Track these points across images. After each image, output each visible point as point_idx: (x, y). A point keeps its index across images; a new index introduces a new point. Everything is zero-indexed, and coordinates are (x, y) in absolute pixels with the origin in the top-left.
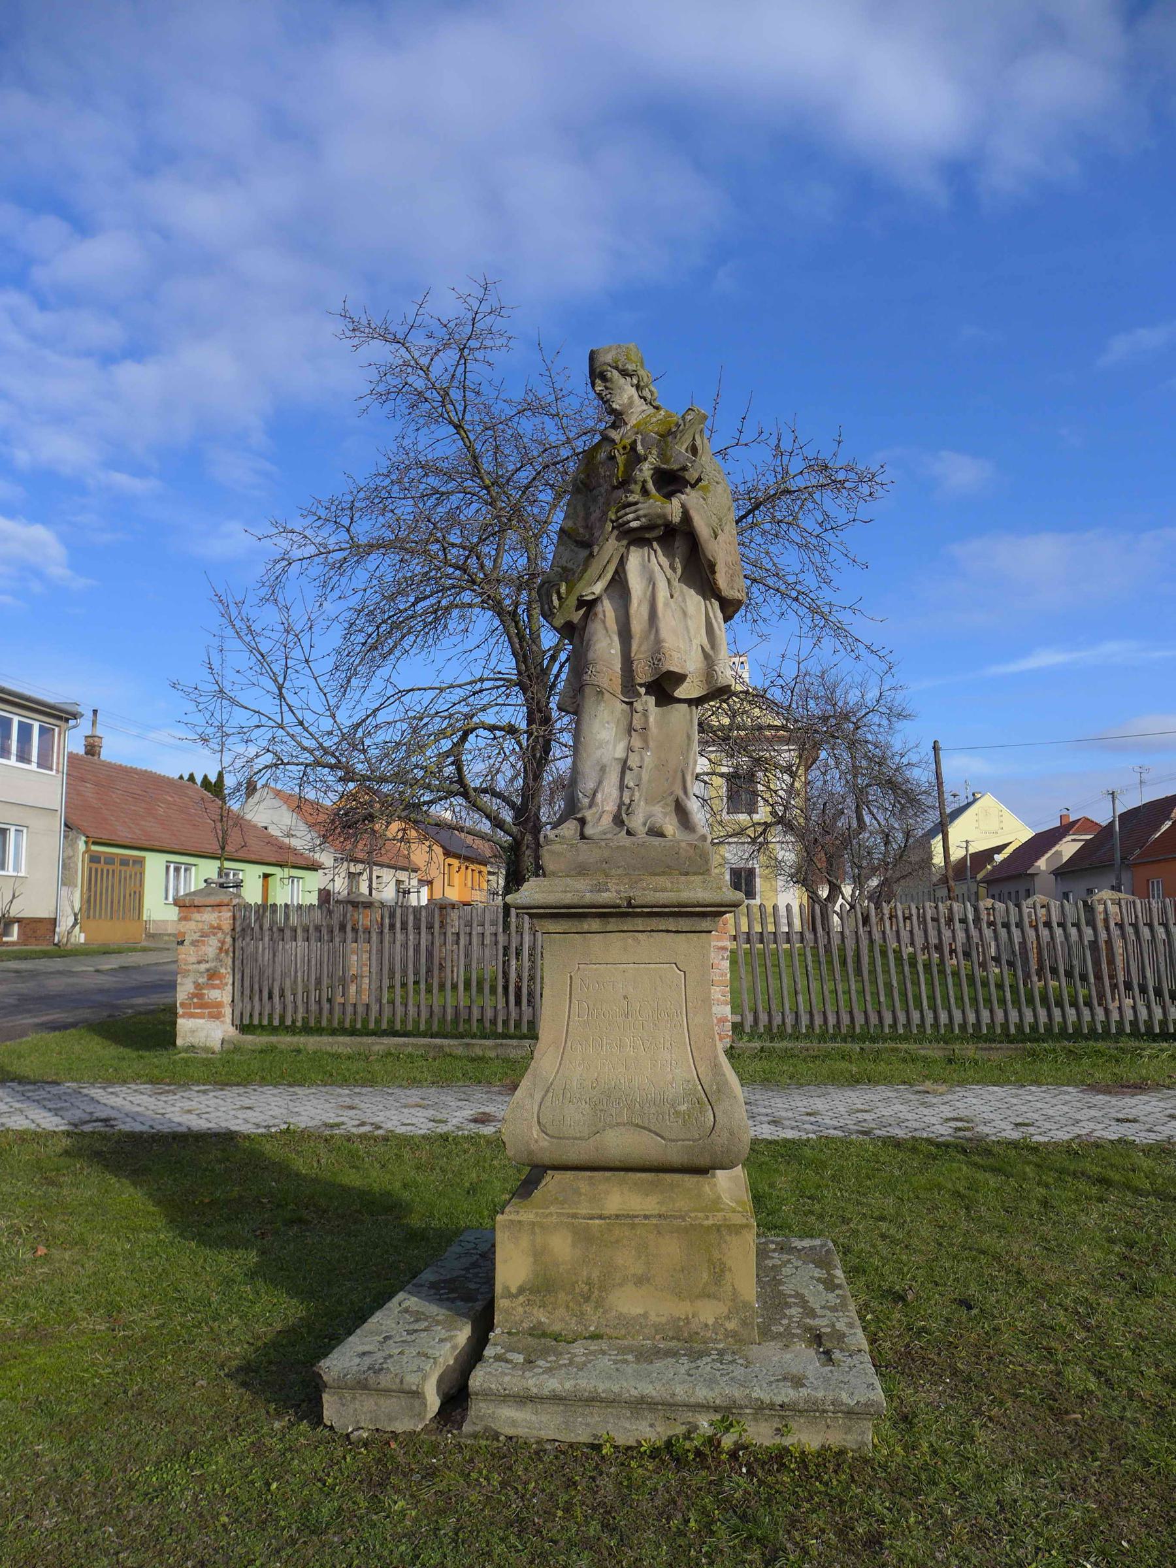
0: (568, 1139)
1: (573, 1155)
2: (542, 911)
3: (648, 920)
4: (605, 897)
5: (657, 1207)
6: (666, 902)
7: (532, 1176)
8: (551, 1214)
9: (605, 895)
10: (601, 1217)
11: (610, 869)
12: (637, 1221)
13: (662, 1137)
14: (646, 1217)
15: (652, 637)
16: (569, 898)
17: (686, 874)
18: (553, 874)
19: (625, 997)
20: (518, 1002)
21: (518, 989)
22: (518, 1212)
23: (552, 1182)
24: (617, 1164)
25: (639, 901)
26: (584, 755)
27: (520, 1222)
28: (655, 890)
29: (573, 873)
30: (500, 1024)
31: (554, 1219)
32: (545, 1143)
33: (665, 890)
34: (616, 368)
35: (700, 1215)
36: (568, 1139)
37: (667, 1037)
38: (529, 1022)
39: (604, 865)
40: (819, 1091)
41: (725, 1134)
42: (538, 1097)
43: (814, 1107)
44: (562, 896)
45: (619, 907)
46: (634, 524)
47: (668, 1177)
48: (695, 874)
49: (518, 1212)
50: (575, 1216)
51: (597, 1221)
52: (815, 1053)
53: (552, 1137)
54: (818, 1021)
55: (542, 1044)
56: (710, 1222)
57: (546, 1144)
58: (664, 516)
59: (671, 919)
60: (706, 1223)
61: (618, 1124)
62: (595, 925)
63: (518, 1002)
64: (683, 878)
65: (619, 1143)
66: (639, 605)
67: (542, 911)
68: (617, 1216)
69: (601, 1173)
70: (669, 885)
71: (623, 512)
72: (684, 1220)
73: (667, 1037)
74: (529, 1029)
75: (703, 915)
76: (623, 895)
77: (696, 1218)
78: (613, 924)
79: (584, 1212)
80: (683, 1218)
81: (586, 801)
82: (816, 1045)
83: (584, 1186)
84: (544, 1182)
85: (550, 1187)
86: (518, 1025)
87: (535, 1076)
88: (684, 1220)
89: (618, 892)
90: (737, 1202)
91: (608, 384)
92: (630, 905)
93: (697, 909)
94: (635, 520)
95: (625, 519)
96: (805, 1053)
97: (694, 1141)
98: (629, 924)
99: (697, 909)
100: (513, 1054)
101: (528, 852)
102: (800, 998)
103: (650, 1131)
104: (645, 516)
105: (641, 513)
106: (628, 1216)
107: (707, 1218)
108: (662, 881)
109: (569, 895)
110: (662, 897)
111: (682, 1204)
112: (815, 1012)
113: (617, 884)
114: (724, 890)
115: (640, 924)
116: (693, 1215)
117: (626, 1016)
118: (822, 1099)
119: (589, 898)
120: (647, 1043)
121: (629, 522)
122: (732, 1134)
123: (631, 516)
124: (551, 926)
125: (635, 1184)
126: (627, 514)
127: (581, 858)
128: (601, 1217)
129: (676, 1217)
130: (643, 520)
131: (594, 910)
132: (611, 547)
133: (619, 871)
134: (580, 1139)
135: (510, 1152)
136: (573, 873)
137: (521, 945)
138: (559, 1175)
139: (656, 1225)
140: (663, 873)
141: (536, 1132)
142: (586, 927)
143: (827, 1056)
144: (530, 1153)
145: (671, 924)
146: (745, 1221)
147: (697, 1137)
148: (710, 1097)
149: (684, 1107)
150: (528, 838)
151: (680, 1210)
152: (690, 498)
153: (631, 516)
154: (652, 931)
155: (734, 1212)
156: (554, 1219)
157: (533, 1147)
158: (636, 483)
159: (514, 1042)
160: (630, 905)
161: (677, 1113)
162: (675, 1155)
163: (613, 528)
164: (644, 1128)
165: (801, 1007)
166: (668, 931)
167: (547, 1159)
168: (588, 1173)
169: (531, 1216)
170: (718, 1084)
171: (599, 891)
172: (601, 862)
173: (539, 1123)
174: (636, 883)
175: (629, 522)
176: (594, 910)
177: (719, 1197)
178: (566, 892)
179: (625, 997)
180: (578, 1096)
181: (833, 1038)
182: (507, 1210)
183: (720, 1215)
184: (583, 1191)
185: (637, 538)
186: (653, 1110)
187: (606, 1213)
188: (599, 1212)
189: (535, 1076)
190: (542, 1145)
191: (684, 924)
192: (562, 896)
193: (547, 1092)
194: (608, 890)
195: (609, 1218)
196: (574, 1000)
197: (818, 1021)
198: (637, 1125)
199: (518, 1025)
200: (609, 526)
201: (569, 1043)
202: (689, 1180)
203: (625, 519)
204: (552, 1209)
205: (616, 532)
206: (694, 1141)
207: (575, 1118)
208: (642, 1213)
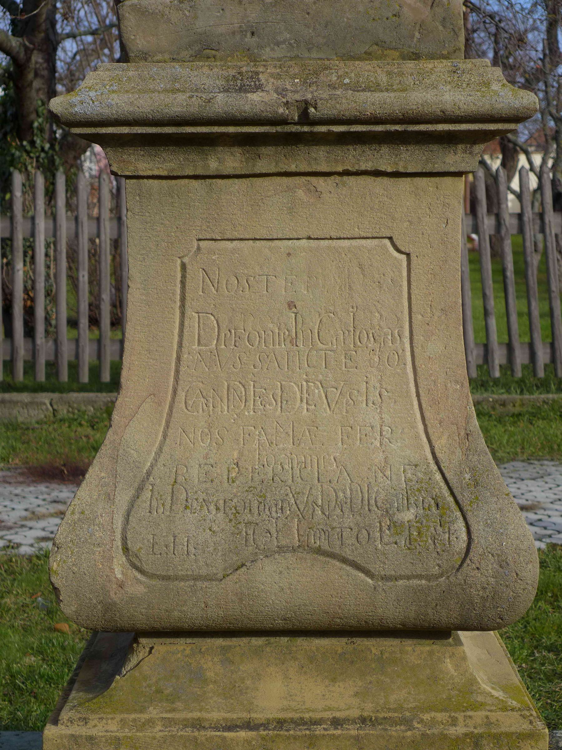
0: (183, 579)
1: (192, 611)
2: (125, 130)
3: (338, 151)
4: (256, 102)
5: (355, 702)
6: (379, 112)
7: (107, 651)
8: (151, 722)
9: (255, 97)
10: (248, 725)
11: (260, 47)
12: (319, 730)
13: (367, 573)
14: (336, 723)
16: (179, 104)
17: (416, 57)
18: (145, 56)
19: (291, 305)
20: (30, 332)
21: (30, 312)
22: (85, 721)
23: (150, 661)
24: (279, 624)
25: (326, 109)
27: (90, 738)
28: (356, 88)
29: (185, 54)
30: (20, 367)
31: (158, 731)
32: (138, 587)
33: (377, 88)
35: (440, 716)
36: (183, 579)
37: (374, 381)
38: (49, 364)
39: (248, 39)
40: (531, 470)
41: (490, 566)
42: (123, 498)
43: (529, 496)
44: (168, 99)
45: (283, 122)
47: (374, 646)
48: (432, 57)
49: (85, 721)
50: (198, 724)
51: (242, 734)
52: (517, 410)
53: (152, 576)
54: (521, 357)
55: (126, 400)
56: (460, 730)
57: (139, 590)
59: (385, 149)
60: (453, 731)
61: (281, 549)
62: (231, 160)
63: (30, 332)
64: (410, 65)
65: (283, 584)
67: (125, 130)
68: (281, 723)
69: (245, 640)
70: (383, 79)
72: (411, 728)
73: (374, 381)
74: (48, 376)
75: (449, 140)
76: (292, 97)
77: (433, 723)
78: (268, 159)
79: (215, 716)
80: (407, 723)
82: (517, 397)
83: (212, 667)
84: (134, 660)
85: (145, 667)
86: (30, 367)
87: (115, 459)
88: (411, 728)
89: (281, 92)
90: (504, 689)
92: (305, 118)
93: (441, 127)
96: (500, 409)
97: (428, 578)
98: (300, 159)
99: (441, 127)
100: (22, 416)
101: (37, 84)
102: (493, 322)
103: (344, 560)
106: (301, 722)
107: (454, 722)
108: (367, 70)
109: (181, 98)
110: (372, 102)
111: (401, 695)
112: (516, 344)
113: (278, 77)
114: (495, 87)
115: (321, 158)
116: (426, 717)
117: (294, 342)
118: (540, 482)
119: (223, 103)
120: (334, 394)
122: (503, 564)
124: (142, 163)
125: (312, 659)
127: (201, 25)
128: (248, 725)
129: (394, 722)
131: (231, 129)
133: (279, 53)
134: (209, 578)
135: (69, 607)
136: (185, 54)
137: (33, 235)
138: (163, 647)
139: (357, 738)
140: (368, 56)
141: (119, 567)
142: (213, 165)
143: (535, 414)
144: (109, 607)
145: (384, 158)
146: (526, 726)
147: (436, 570)
148: (457, 499)
149: (408, 515)
150: (37, 59)
151: (400, 708)
154: (347, 173)
155: (505, 709)
156: (158, 731)
157: (115, 596)
159: (25, 397)
160: (305, 118)
161: (395, 526)
162: (390, 606)
164: (332, 556)
165: (494, 337)
166: (377, 173)
167: (140, 617)
168: (220, 642)
169: (113, 726)
170: (473, 470)
171: (242, 89)
172: (242, 32)
173: (126, 549)
174: (316, 73)
176: (231, 129)
177: (472, 681)
178: (174, 91)
179: (291, 305)
180: (202, 496)
181: (543, 385)
182: (65, 715)
183: (479, 715)
184: (210, 674)
186: (349, 521)
187: (258, 716)
188: (245, 715)
189: (115, 459)
190: (131, 592)
191: (410, 158)
192: (168, 99)
193: (140, 489)
194: (259, 87)
195: (265, 725)
196: (189, 312)
197: (521, 357)
198: (319, 551)
199: (30, 367)
201: (181, 395)
202: (414, 651)
204: (153, 712)
206: (428, 578)
207: (199, 536)
208: (328, 715)
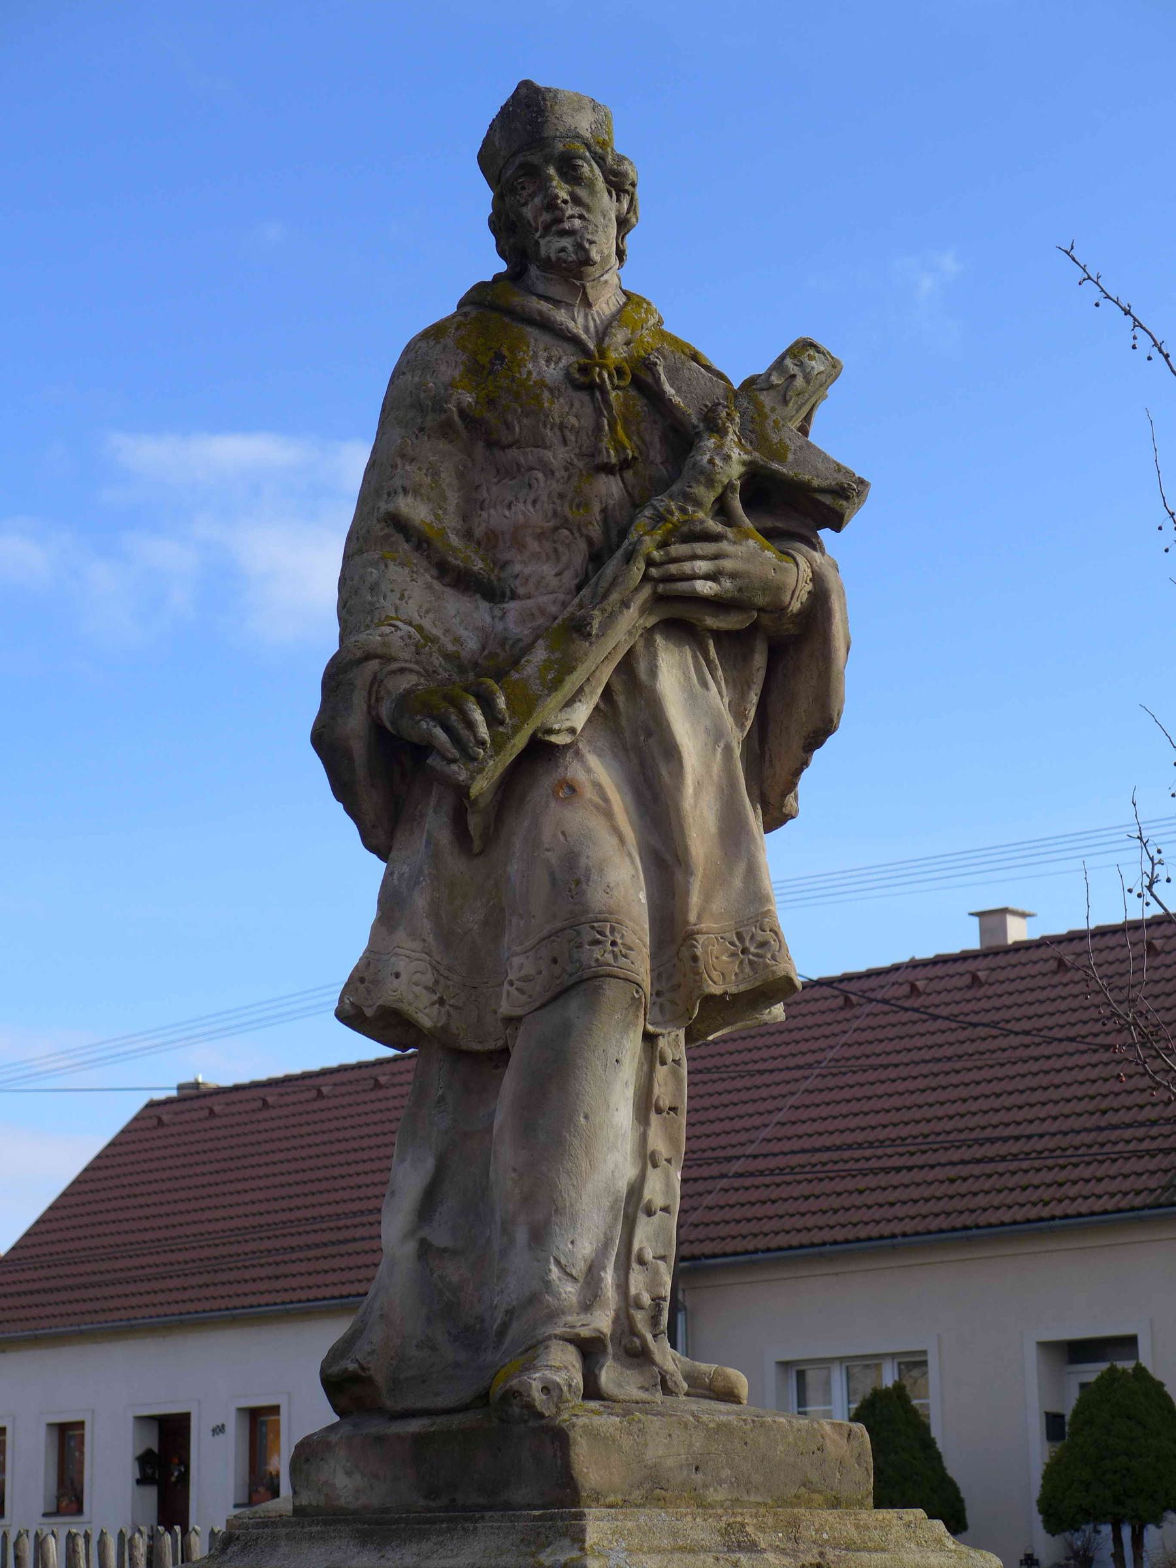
15: (738, 883)
26: (584, 1164)
29: (637, 1495)
34: (600, 160)
46: (705, 588)
58: (779, 589)
66: (697, 794)
71: (678, 549)
81: (569, 1292)
91: (582, 193)
94: (707, 577)
95: (687, 567)
104: (733, 576)
105: (727, 564)
121: (694, 577)
123: (702, 566)
126: (694, 557)
130: (727, 584)
132: (628, 624)
152: (402, 495)
153: (702, 566)
158: (710, 483)
163: (646, 578)
175: (694, 577)
185: (679, 617)
200: (638, 569)
203: (687, 567)
205: (647, 591)
